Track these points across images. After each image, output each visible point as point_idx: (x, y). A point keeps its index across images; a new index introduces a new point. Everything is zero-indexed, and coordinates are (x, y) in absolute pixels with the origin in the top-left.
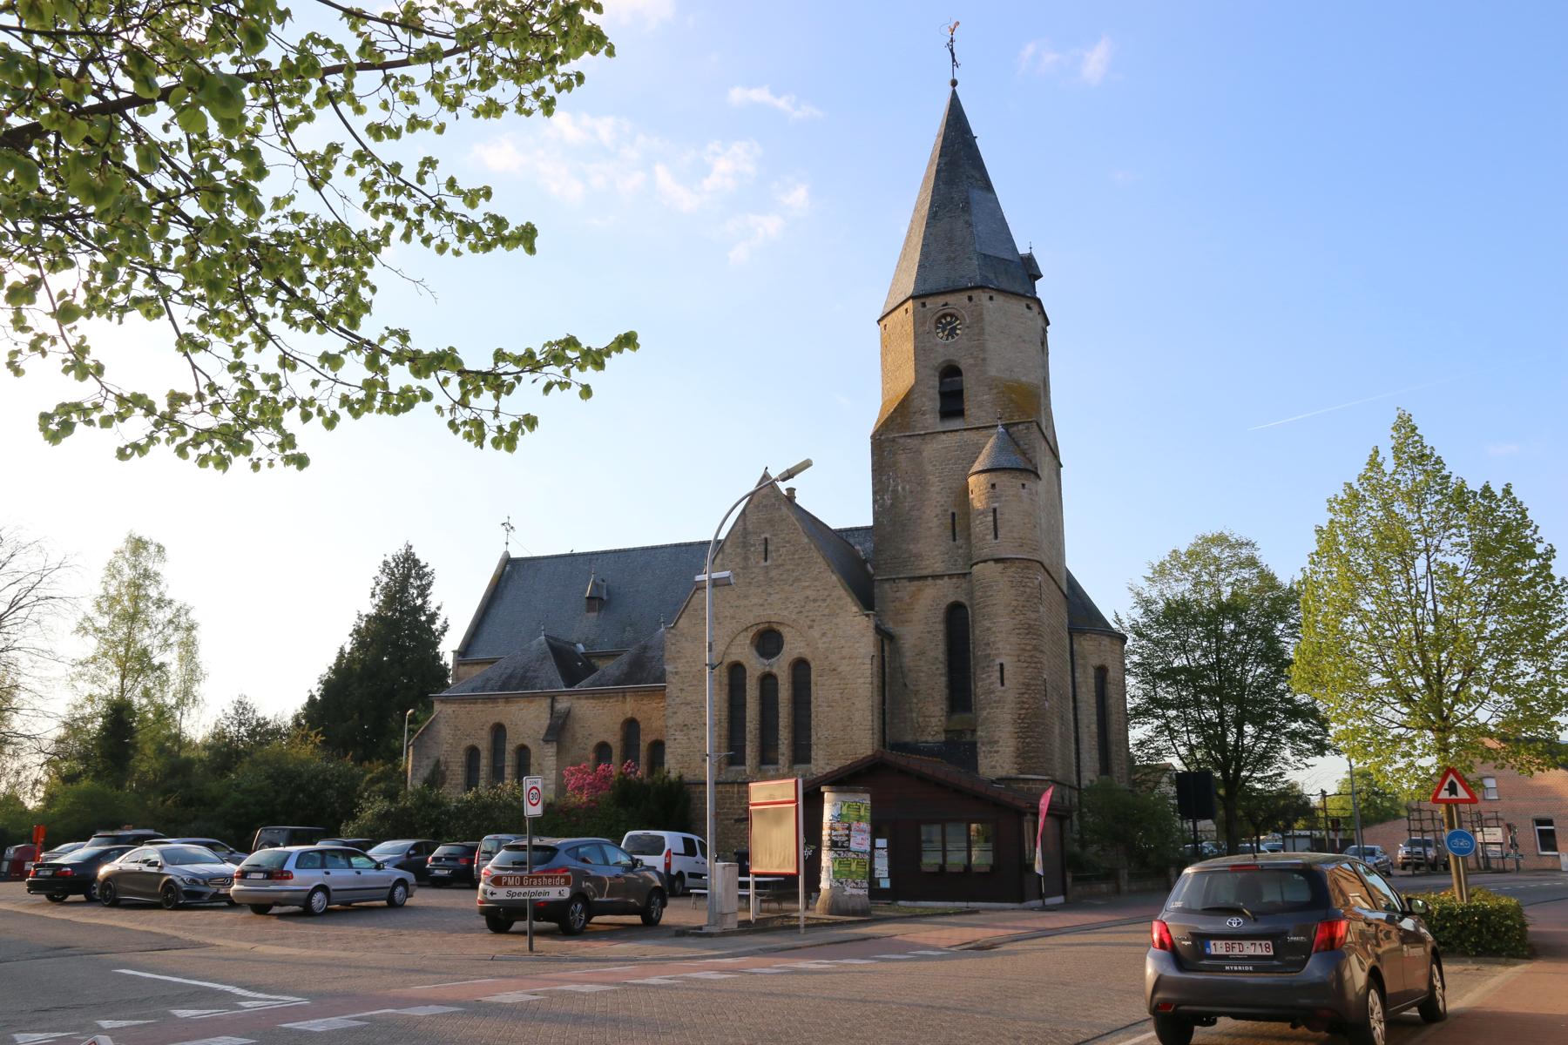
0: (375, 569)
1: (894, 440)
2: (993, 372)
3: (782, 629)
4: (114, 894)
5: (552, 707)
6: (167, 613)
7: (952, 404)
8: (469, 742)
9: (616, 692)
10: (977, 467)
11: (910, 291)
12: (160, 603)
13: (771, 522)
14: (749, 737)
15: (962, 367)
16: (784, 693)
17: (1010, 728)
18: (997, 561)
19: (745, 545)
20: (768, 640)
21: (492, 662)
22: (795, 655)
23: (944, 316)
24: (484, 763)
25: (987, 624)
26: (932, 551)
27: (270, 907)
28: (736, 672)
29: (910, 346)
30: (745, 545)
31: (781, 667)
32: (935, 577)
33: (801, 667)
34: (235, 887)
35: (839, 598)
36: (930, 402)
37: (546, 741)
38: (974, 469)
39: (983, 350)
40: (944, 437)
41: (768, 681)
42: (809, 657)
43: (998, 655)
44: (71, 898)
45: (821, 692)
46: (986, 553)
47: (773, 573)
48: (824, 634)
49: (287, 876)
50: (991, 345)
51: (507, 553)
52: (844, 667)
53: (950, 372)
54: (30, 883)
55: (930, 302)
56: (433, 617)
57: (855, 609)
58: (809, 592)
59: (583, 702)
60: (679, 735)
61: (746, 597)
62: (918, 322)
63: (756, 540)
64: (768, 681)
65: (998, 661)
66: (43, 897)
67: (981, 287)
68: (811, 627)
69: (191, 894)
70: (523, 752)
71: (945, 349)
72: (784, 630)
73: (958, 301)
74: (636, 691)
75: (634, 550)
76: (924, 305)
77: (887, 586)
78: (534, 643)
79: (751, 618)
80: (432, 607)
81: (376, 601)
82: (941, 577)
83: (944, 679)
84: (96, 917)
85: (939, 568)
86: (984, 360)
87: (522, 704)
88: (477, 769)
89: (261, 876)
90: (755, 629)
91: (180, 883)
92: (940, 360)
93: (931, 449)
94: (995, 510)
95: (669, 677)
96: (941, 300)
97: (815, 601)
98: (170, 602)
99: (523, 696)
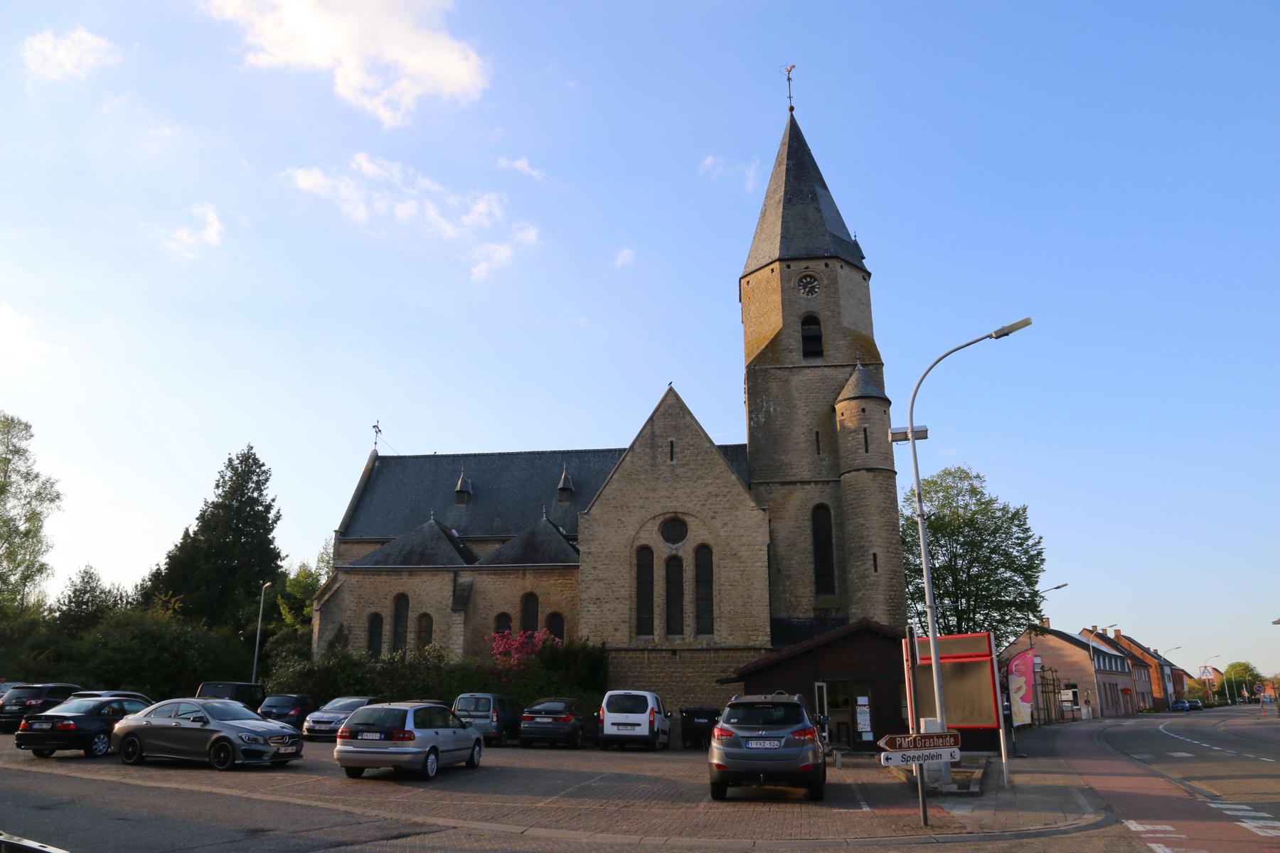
0: (221, 465)
1: (766, 370)
2: (845, 324)
3: (686, 518)
4: (139, 750)
5: (455, 581)
6: (34, 487)
7: (813, 345)
8: (373, 610)
9: (517, 570)
10: (846, 393)
11: (777, 255)
12: (28, 477)
13: (676, 428)
14: (657, 610)
15: (821, 317)
16: (689, 573)
17: (883, 607)
18: (868, 470)
19: (653, 446)
20: (674, 528)
21: (382, 542)
22: (699, 540)
23: (805, 277)
24: (387, 628)
25: (861, 521)
26: (800, 459)
27: (362, 770)
28: (644, 555)
29: (777, 298)
30: (653, 446)
31: (686, 551)
32: (803, 483)
33: (704, 552)
34: (339, 746)
35: (738, 495)
36: (795, 342)
37: (454, 610)
38: (840, 398)
39: (838, 305)
40: (808, 371)
41: (674, 563)
42: (711, 543)
43: (872, 547)
44: (58, 753)
45: (723, 573)
46: (859, 462)
47: (679, 471)
48: (725, 524)
49: (410, 737)
50: (843, 302)
51: (375, 452)
52: (743, 553)
53: (810, 321)
54: (18, 737)
55: (793, 265)
56: (268, 508)
57: (752, 504)
58: (711, 489)
59: (484, 577)
60: (592, 608)
61: (654, 490)
62: (784, 279)
63: (663, 443)
64: (674, 563)
65: (872, 551)
66: (29, 753)
67: (836, 257)
68: (713, 518)
69: (249, 754)
70: (425, 619)
71: (806, 303)
72: (690, 521)
73: (817, 266)
74: (536, 570)
75: (492, 455)
76: (789, 267)
77: (762, 488)
78: (425, 525)
79: (659, 509)
80: (268, 500)
81: (220, 491)
82: (809, 483)
83: (812, 566)
84: (150, 778)
85: (806, 475)
86: (839, 313)
87: (425, 577)
88: (380, 634)
89: (377, 736)
90: (662, 518)
91: (238, 741)
92: (804, 310)
93: (797, 380)
94: (865, 430)
95: (583, 557)
96: (803, 264)
97: (716, 496)
98: (37, 476)
99: (426, 570)
